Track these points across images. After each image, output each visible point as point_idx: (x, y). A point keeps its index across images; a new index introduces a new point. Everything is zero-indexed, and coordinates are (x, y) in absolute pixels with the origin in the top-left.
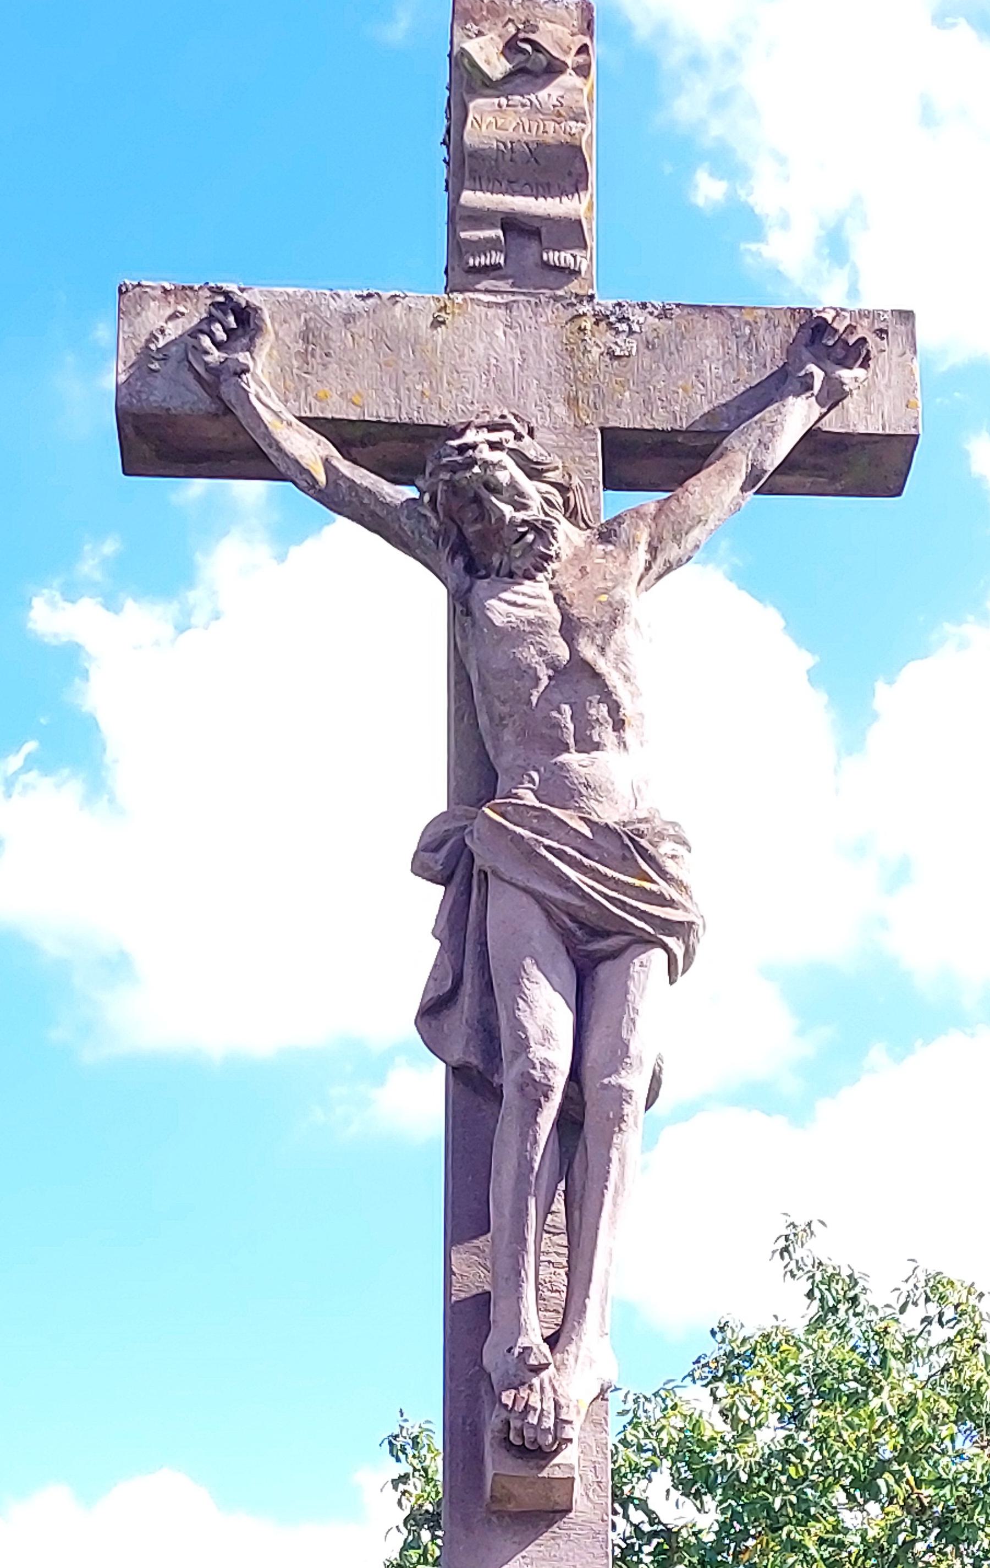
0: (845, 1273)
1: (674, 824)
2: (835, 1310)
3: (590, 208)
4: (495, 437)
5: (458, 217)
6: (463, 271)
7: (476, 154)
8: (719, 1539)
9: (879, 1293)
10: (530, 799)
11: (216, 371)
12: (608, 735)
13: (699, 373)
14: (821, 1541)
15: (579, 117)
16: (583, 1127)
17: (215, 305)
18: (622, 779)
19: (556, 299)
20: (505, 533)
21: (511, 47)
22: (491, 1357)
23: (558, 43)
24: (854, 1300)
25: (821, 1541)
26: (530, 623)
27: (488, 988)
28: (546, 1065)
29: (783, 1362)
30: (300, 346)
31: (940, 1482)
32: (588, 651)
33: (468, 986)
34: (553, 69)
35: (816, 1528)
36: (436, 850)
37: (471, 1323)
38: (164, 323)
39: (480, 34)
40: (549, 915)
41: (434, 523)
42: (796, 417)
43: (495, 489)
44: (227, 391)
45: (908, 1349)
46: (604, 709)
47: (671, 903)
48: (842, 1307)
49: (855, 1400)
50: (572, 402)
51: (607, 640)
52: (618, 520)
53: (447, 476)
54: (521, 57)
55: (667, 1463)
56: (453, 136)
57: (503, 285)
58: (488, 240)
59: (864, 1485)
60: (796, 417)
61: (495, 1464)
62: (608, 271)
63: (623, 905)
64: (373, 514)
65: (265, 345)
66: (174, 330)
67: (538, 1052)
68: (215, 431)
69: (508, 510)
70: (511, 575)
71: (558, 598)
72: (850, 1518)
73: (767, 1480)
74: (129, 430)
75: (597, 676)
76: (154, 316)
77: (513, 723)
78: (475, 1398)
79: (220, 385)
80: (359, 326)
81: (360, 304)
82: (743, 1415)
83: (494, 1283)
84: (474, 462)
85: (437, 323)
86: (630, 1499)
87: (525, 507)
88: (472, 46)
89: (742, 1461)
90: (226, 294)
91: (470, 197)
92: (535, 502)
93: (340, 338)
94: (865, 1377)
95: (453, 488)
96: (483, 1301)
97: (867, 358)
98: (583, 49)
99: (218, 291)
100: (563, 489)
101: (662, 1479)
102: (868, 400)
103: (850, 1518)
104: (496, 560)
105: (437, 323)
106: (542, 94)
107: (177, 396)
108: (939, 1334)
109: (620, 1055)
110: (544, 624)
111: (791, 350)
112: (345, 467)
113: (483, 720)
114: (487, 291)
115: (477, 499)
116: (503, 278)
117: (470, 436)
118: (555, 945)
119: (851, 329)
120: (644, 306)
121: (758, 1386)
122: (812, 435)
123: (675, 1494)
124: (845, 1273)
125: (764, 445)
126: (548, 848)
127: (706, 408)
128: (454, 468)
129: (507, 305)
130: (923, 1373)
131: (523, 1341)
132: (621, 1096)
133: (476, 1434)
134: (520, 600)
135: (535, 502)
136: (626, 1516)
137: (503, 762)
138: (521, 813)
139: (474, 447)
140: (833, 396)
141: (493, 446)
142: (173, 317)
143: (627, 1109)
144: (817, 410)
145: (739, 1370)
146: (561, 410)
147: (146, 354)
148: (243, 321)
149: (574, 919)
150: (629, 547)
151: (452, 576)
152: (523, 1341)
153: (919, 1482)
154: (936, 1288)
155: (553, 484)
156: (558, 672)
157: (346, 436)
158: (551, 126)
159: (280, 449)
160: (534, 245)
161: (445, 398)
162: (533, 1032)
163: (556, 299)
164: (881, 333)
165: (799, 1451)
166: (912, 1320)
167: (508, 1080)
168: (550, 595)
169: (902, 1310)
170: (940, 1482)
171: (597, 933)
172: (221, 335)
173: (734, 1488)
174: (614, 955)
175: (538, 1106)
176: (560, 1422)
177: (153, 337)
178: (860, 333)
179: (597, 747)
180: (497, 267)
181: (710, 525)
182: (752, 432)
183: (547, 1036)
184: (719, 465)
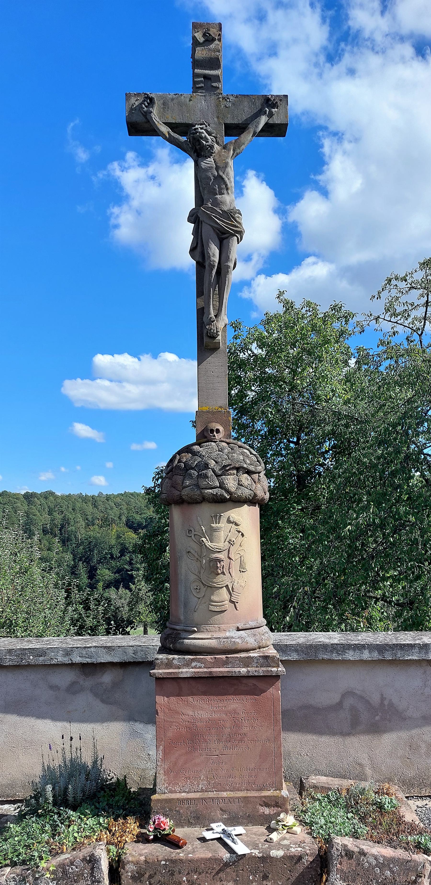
0: (290, 301)
1: (238, 210)
2: (289, 309)
3: (221, 73)
4: (201, 126)
5: (195, 75)
6: (196, 89)
7: (197, 61)
8: (266, 357)
9: (297, 306)
10: (210, 205)
11: (145, 112)
12: (225, 192)
13: (244, 110)
14: (285, 356)
15: (219, 51)
16: (222, 272)
17: (145, 97)
18: (228, 200)
19: (215, 94)
20: (204, 148)
21: (204, 35)
22: (205, 319)
23: (214, 33)
24: (292, 307)
25: (285, 356)
26: (209, 167)
27: (203, 246)
28: (214, 261)
29: (279, 320)
30: (163, 106)
31: (308, 344)
32: (221, 173)
33: (199, 245)
34: (213, 40)
35: (284, 353)
36: (192, 216)
37: (201, 312)
38: (135, 102)
39: (198, 32)
40: (214, 230)
41: (190, 146)
42: (263, 120)
43: (202, 138)
44: (148, 117)
45: (303, 317)
46: (224, 186)
47: (237, 227)
48: (290, 308)
49: (292, 327)
50: (218, 117)
51: (225, 171)
52: (227, 144)
53: (192, 135)
54: (207, 37)
55: (255, 342)
56: (193, 56)
57: (204, 91)
58: (201, 81)
59: (293, 345)
60: (263, 120)
61: (206, 340)
62: (225, 88)
63: (228, 228)
64: (178, 144)
65: (156, 107)
66: (137, 103)
67: (212, 258)
68: (146, 125)
69: (204, 142)
70: (206, 157)
71: (215, 162)
72: (291, 351)
73: (275, 344)
74: (129, 126)
75: (223, 179)
76: (133, 100)
77: (208, 188)
78: (202, 327)
79: (147, 115)
80: (174, 101)
81: (174, 96)
82: (270, 331)
83: (205, 305)
84: (197, 132)
85: (190, 100)
86: (248, 349)
87: (208, 142)
88: (196, 35)
89: (269, 341)
90: (147, 95)
91: (197, 71)
92: (210, 140)
93: (171, 104)
94: (294, 323)
95: (194, 138)
96: (203, 308)
97: (278, 106)
98: (220, 35)
99: (146, 94)
100: (216, 138)
101: (255, 345)
102: (278, 116)
103: (291, 351)
104: (203, 153)
105: (190, 100)
106: (211, 46)
107: (139, 118)
108: (309, 314)
109: (228, 259)
110: (212, 167)
111: (262, 105)
112: (172, 133)
113: (201, 188)
114: (200, 93)
115: (199, 141)
116: (203, 89)
117: (197, 126)
118: (215, 236)
119: (274, 100)
120: (232, 95)
121: (273, 325)
122: (267, 124)
123: (257, 348)
124: (290, 301)
125: (257, 127)
126: (214, 216)
127: (245, 118)
128: (193, 134)
129: (204, 96)
130: (306, 322)
131: (210, 316)
132: (228, 267)
133: (202, 333)
134: (207, 162)
135: (210, 140)
136: (247, 352)
137: (205, 197)
138: (208, 208)
139: (197, 129)
140: (271, 115)
141: (201, 128)
142: (137, 100)
143: (229, 270)
144: (267, 118)
145: (270, 322)
146: (216, 119)
147: (131, 109)
148: (151, 101)
149: (219, 231)
150: (229, 150)
151: (194, 157)
152: (210, 316)
153: (304, 344)
154: (309, 304)
155: (214, 137)
156: (215, 178)
157: (172, 126)
158: (213, 53)
159: (159, 130)
160: (210, 81)
161: (192, 117)
162: (211, 254)
163: (215, 94)
164: (281, 100)
165: (281, 338)
166: (304, 311)
167: (207, 264)
168: (213, 161)
169: (302, 309)
170: (308, 344)
171: (223, 233)
172: (147, 104)
173: (269, 346)
174: (227, 238)
175: (212, 270)
176: (217, 332)
177: (133, 105)
178: (276, 101)
179: (223, 194)
180: (202, 87)
181: (246, 145)
182: (254, 123)
183: (214, 255)
184: (247, 131)
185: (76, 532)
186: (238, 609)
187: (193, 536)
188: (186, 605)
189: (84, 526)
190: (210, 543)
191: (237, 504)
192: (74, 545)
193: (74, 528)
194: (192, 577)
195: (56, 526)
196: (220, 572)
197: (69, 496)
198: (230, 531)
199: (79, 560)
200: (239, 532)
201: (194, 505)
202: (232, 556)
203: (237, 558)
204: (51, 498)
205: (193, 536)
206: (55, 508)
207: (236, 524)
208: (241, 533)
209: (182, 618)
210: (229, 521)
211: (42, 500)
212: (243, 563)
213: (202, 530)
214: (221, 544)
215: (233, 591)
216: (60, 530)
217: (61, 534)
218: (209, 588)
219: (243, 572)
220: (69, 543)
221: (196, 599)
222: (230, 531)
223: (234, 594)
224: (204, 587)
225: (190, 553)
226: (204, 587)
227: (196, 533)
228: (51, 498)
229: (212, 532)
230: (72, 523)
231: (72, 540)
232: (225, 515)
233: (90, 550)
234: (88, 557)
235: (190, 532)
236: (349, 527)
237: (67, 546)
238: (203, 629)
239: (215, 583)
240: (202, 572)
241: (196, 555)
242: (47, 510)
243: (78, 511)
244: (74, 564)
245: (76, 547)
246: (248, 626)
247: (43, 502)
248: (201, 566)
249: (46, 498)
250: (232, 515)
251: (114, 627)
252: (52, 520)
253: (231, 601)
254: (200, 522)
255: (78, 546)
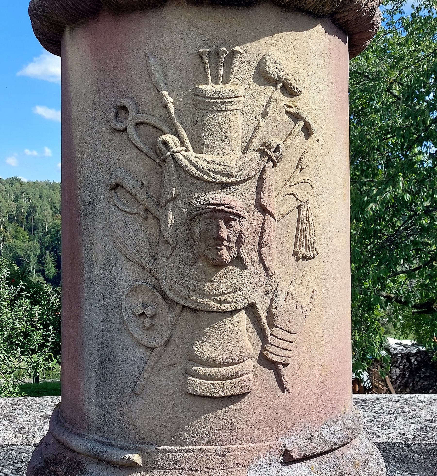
185: (43, 221)
186: (288, 386)
187: (131, 130)
188: (105, 370)
189: (51, 214)
190: (191, 155)
191: (292, 18)
192: (41, 234)
193: (41, 216)
194: (129, 274)
195: (23, 214)
196: (226, 255)
197: (36, 183)
198: (265, 113)
199: (46, 250)
200: (296, 117)
201: (137, 15)
202: (271, 200)
203: (286, 209)
204: (18, 184)
205: (131, 130)
206: (21, 195)
207: (288, 90)
208: (301, 124)
209: (92, 411)
210: (263, 76)
211: (7, 185)
212: (305, 230)
213: (165, 106)
214: (233, 159)
215: (272, 325)
216: (27, 218)
217: (27, 223)
218: (187, 316)
219: (305, 258)
220: (35, 232)
221: (141, 351)
222: (265, 113)
223: (276, 336)
224: (171, 310)
225: (120, 191)
226: (171, 310)
227: (142, 118)
228: (18, 184)
229: (202, 110)
230: (39, 211)
231: (39, 229)
232: (252, 51)
233: (57, 239)
234: (55, 246)
235: (122, 113)
236: (371, 204)
237: (34, 234)
238: (164, 458)
239: (209, 296)
240: (164, 254)
241: (142, 196)
242: (13, 197)
243: (45, 199)
244: (41, 253)
245: (42, 236)
246: (319, 444)
247: (8, 188)
248: (161, 237)
249: (12, 184)
250: (275, 54)
251: (53, 333)
252: (18, 207)
253: (265, 361)
254: (159, 78)
255: (45, 234)
